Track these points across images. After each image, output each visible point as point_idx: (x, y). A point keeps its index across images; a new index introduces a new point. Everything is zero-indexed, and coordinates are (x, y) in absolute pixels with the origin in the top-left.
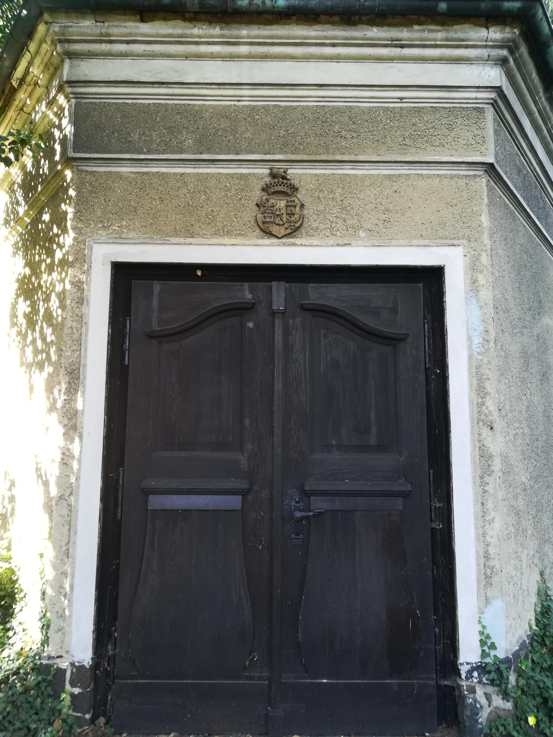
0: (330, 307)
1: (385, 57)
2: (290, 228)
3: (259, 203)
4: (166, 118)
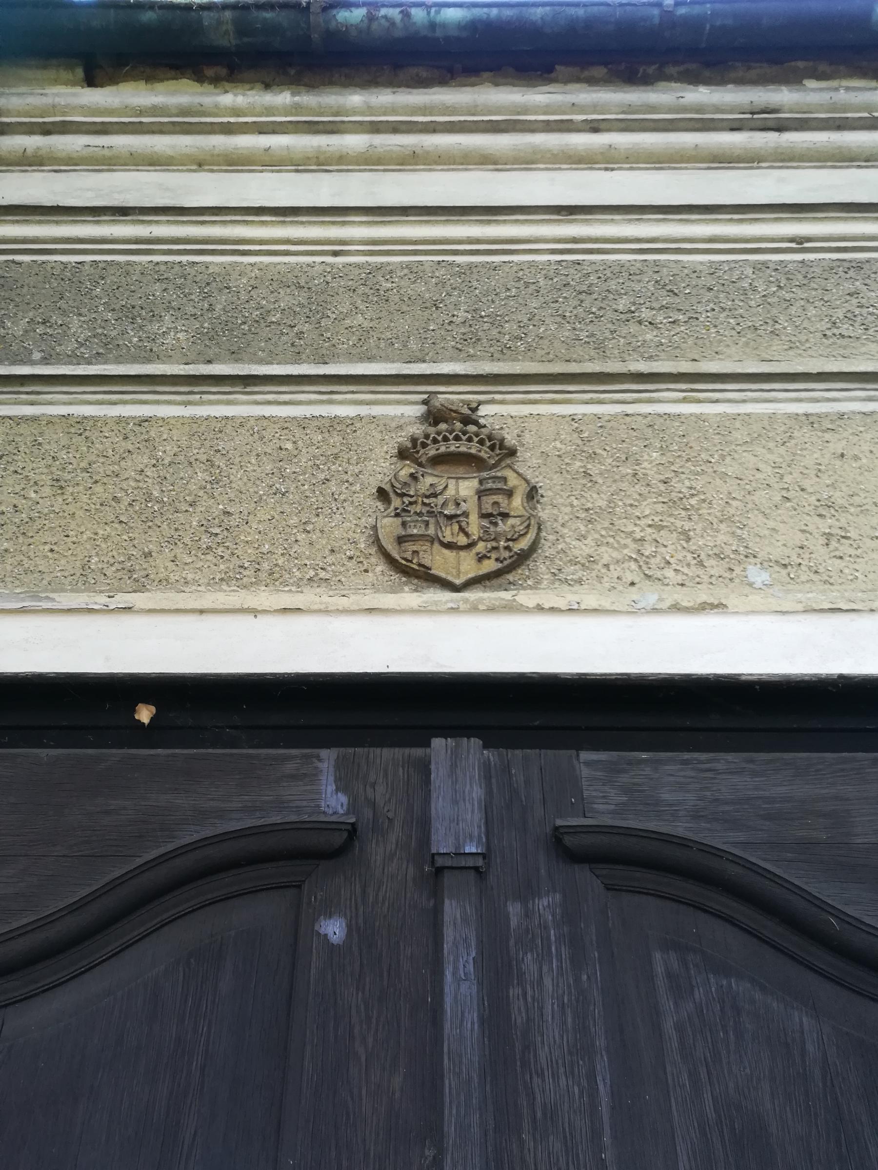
0: (683, 843)
1: (737, 152)
2: (494, 555)
3: (387, 487)
4: (121, 289)
